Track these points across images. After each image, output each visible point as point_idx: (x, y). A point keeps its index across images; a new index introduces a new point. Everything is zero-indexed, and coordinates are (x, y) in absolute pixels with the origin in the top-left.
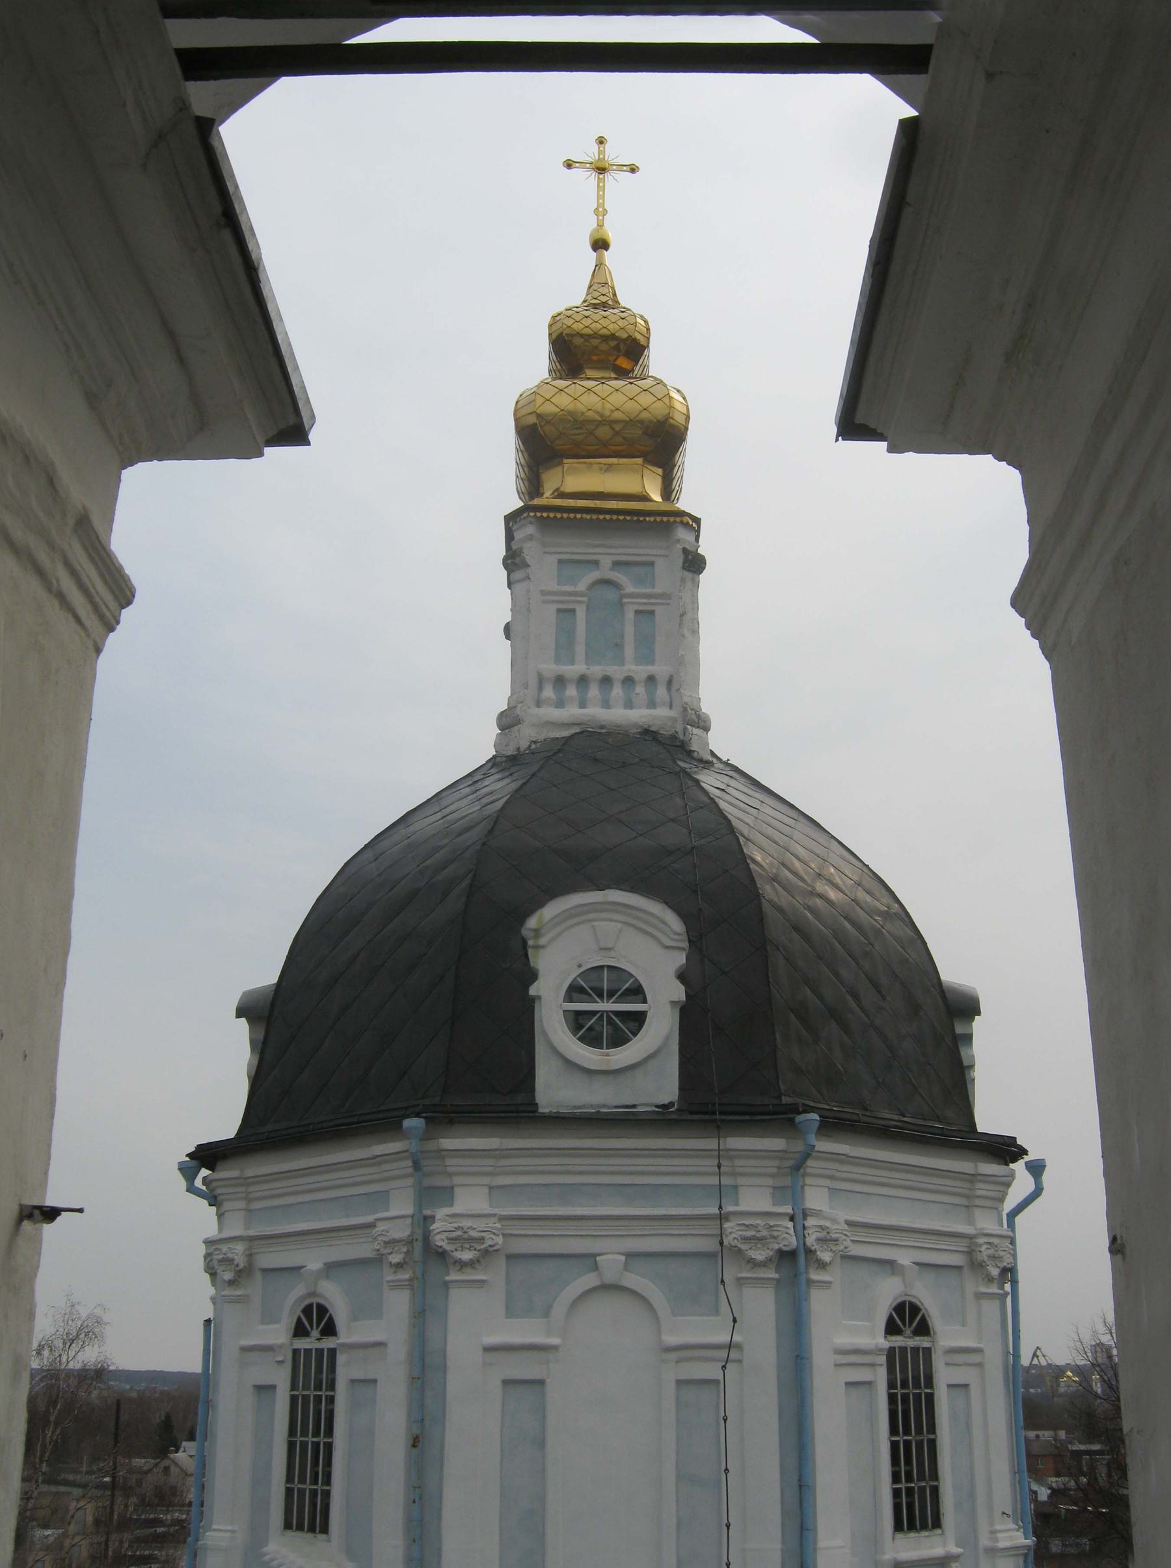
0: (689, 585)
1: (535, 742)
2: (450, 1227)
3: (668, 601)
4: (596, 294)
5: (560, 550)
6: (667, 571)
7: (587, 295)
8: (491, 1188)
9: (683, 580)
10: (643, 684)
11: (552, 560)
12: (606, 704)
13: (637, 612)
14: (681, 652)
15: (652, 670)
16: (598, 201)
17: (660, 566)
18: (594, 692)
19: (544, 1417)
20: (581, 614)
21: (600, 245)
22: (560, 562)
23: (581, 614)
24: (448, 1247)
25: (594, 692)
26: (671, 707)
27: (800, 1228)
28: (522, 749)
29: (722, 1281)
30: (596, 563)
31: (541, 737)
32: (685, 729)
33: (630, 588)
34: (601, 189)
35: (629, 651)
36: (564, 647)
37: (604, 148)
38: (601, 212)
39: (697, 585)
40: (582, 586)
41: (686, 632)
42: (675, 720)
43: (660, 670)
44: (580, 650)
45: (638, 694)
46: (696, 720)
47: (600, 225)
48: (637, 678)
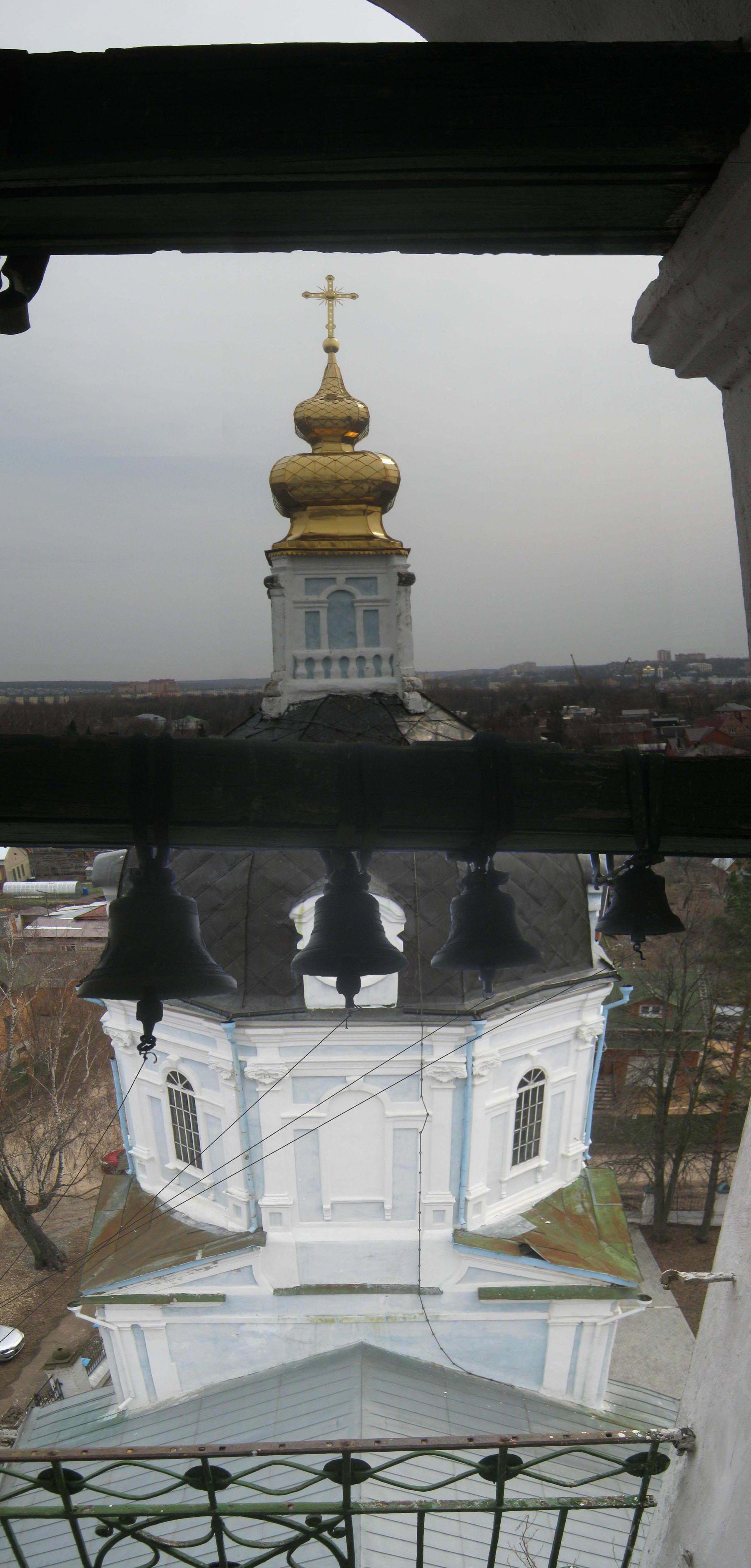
0: (403, 594)
1: (293, 705)
2: (256, 1069)
3: (388, 604)
4: (329, 386)
5: (304, 572)
6: (386, 585)
7: (322, 385)
8: (280, 1048)
9: (399, 593)
10: (372, 661)
11: (301, 580)
12: (345, 675)
13: (365, 611)
14: (399, 641)
15: (376, 650)
16: (329, 319)
17: (381, 579)
18: (335, 667)
19: (318, 1144)
20: (323, 614)
21: (331, 349)
22: (306, 579)
23: (323, 614)
24: (256, 1078)
25: (335, 667)
26: (393, 674)
27: (470, 1067)
28: (282, 713)
29: (421, 1096)
30: (334, 579)
31: (297, 700)
32: (404, 696)
33: (359, 596)
34: (331, 311)
35: (361, 638)
36: (312, 637)
37: (332, 283)
38: (331, 326)
39: (408, 592)
40: (323, 597)
41: (402, 626)
42: (396, 685)
43: (384, 650)
44: (324, 638)
45: (368, 668)
46: (412, 687)
47: (331, 337)
48: (366, 656)
